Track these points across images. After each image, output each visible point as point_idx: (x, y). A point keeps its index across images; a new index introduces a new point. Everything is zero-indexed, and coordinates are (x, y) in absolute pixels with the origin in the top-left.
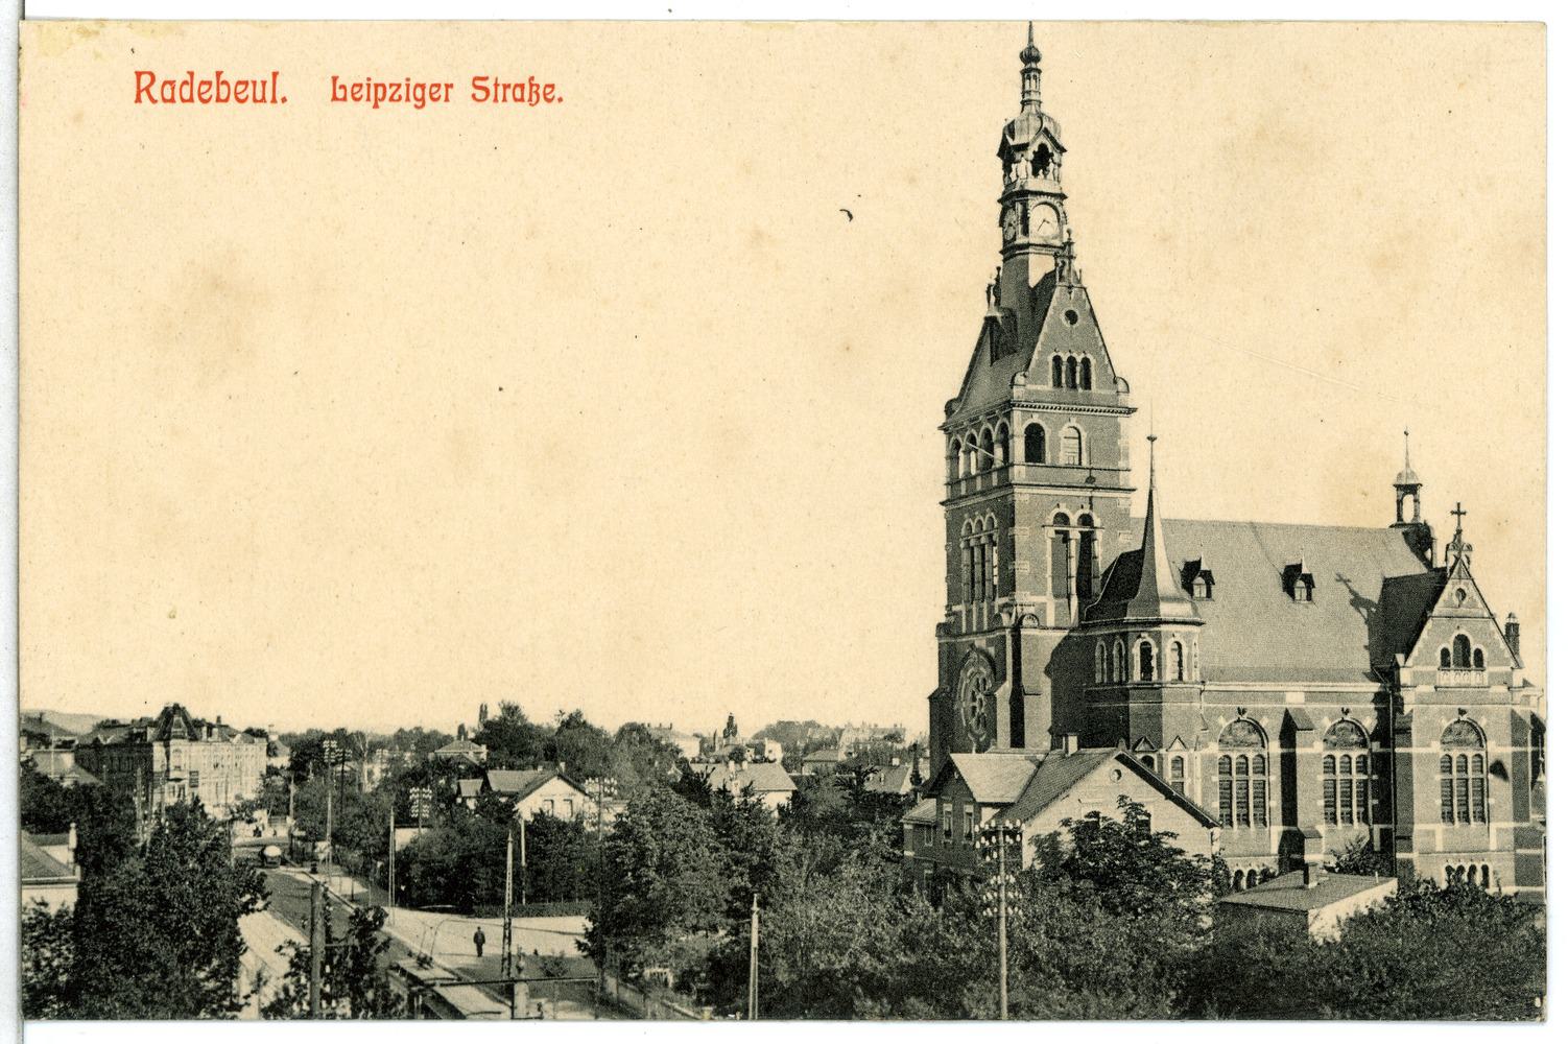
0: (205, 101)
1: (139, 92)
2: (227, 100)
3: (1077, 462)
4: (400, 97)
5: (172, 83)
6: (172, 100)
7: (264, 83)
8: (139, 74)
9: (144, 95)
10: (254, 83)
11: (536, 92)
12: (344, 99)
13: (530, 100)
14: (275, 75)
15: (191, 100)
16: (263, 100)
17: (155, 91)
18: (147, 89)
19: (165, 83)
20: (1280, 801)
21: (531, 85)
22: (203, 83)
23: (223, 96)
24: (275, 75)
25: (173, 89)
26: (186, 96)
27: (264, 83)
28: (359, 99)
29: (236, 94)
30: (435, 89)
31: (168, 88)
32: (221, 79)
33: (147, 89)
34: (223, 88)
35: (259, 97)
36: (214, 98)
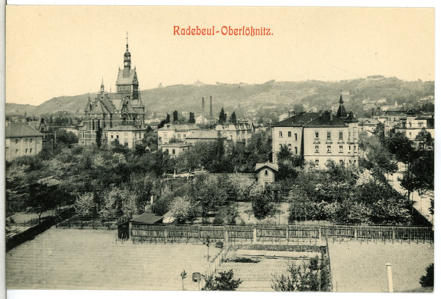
0: (194, 34)
1: (175, 32)
2: (199, 34)
3: (137, 235)
4: (270, 33)
5: (184, 29)
6: (184, 34)
7: (210, 29)
8: (175, 27)
9: (176, 33)
10: (208, 29)
11: (254, 32)
12: (184, 34)
13: (251, 34)
14: (214, 27)
15: (189, 34)
16: (210, 34)
17: (179, 31)
18: (177, 31)
19: (182, 29)
20: (274, 179)
21: (252, 29)
22: (193, 29)
23: (231, 33)
24: (214, 27)
25: (184, 31)
26: (188, 33)
27: (210, 29)
28: (237, 34)
29: (234, 33)
30: (203, 31)
31: (183, 31)
32: (198, 28)
33: (177, 31)
34: (231, 31)
35: (209, 33)
36: (196, 34)
